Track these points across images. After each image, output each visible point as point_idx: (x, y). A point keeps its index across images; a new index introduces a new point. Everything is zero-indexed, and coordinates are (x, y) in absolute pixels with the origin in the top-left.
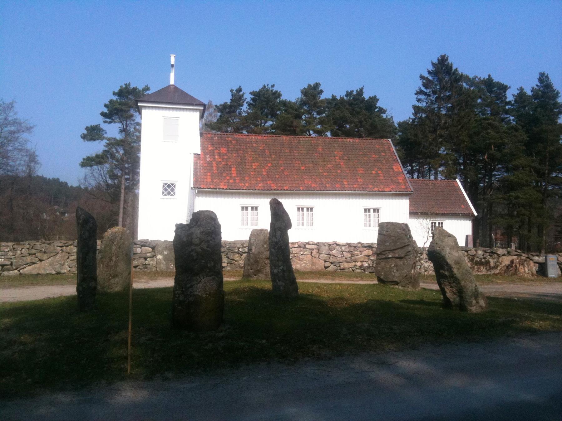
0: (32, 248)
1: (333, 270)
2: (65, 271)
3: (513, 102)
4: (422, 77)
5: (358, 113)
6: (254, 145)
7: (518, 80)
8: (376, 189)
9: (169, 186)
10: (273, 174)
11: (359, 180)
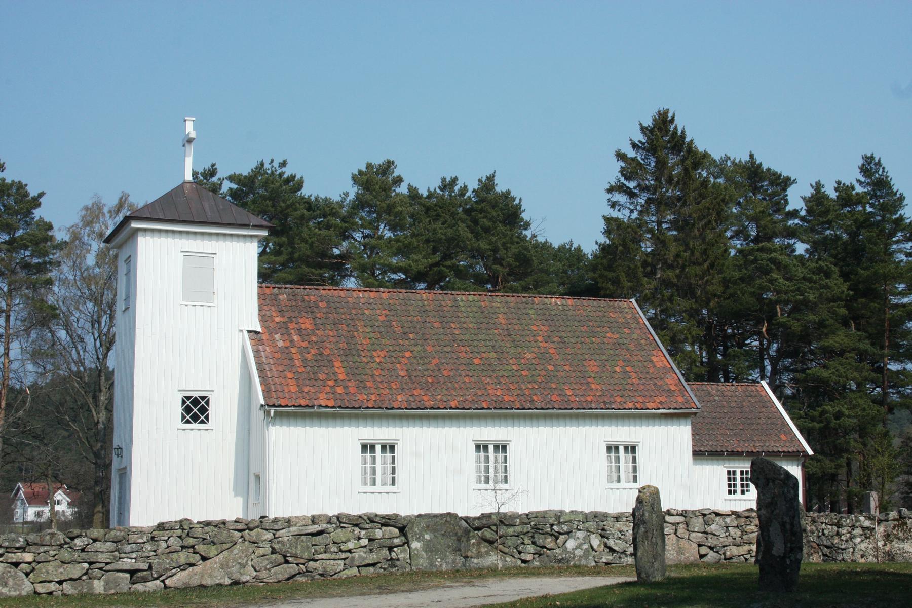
0: (188, 535)
1: (714, 561)
2: (248, 578)
3: (803, 213)
4: (621, 156)
5: (487, 230)
6: (366, 312)
7: (814, 164)
8: (631, 405)
9: (196, 402)
10: (419, 373)
11: (593, 386)
